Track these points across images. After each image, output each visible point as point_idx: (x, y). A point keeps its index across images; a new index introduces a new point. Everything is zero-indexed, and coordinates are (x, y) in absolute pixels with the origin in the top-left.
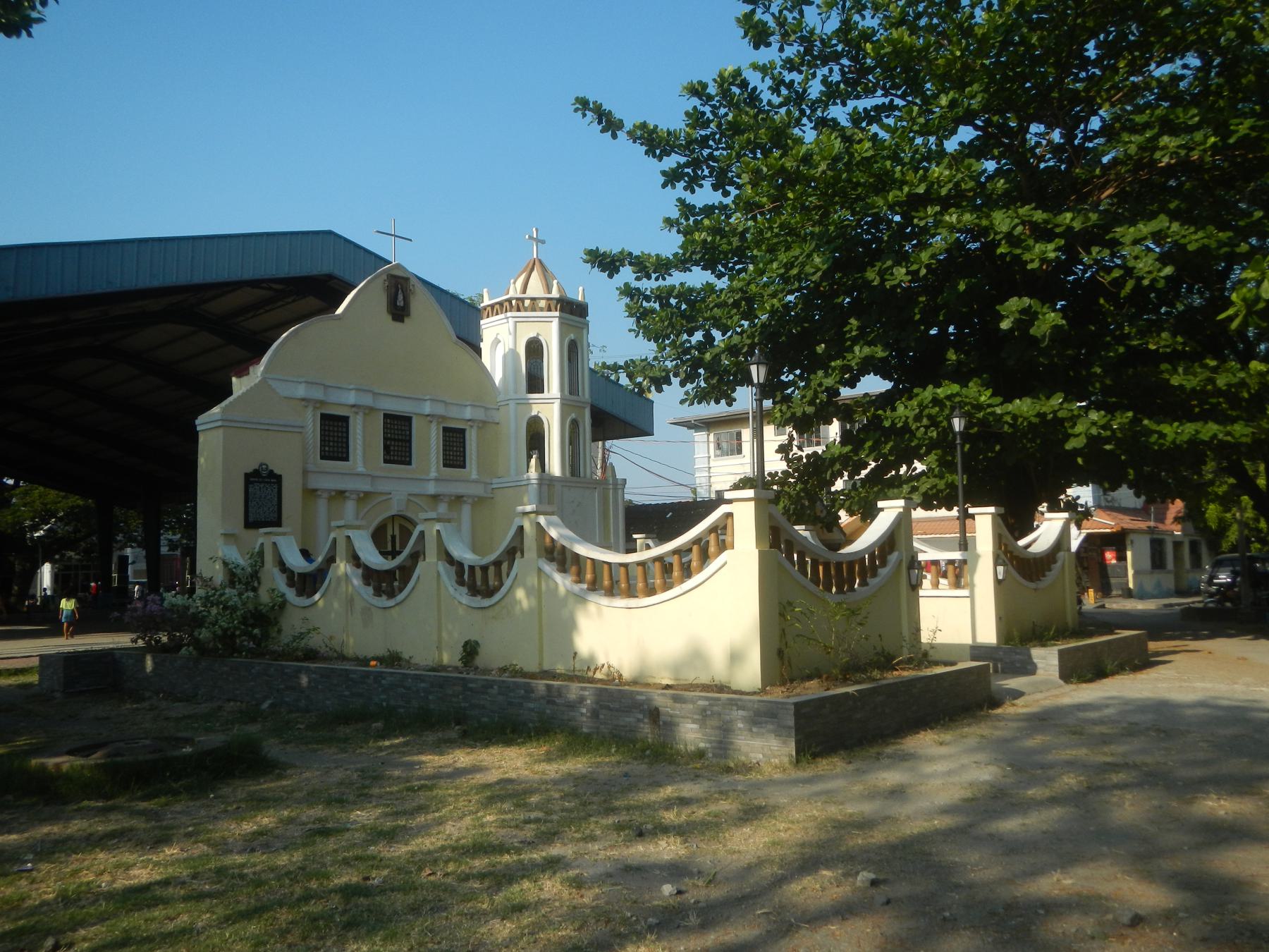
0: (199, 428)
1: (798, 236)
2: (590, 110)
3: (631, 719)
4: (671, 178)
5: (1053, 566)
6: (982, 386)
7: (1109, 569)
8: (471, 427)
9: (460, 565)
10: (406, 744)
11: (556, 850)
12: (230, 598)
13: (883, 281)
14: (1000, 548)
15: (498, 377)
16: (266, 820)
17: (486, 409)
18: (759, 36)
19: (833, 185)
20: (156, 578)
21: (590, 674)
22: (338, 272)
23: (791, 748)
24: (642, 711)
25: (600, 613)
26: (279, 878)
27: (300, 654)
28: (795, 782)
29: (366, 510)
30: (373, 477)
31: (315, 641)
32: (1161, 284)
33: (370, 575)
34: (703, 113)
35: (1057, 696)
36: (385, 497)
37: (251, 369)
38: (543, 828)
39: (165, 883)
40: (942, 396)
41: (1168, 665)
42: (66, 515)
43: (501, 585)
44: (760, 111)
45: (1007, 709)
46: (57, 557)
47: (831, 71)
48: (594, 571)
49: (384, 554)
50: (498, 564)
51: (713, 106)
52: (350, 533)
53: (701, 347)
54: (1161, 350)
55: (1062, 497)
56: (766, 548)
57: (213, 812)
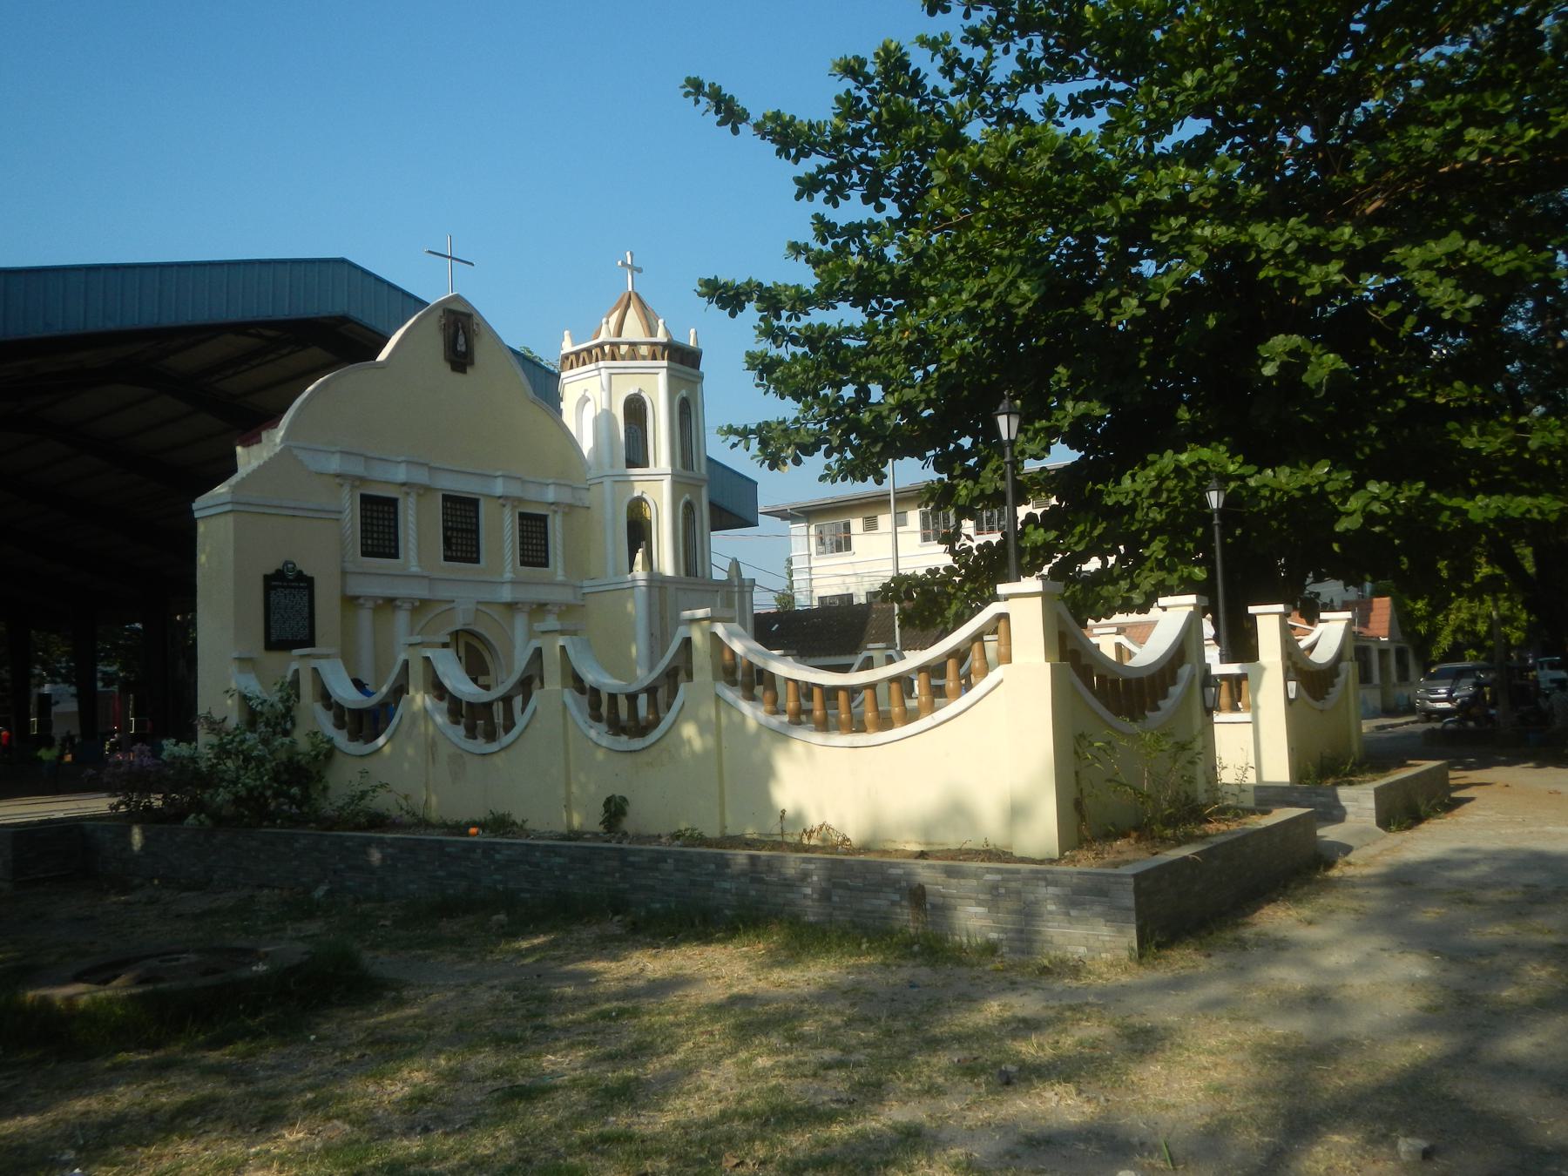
0: (197, 515)
2: (705, 95)
4: (807, 187)
5: (1336, 680)
8: (555, 512)
9: (595, 692)
10: (554, 945)
12: (254, 747)
15: (587, 445)
17: (574, 488)
23: (1131, 937)
24: (899, 890)
25: (810, 754)
27: (363, 820)
29: (423, 622)
30: (431, 579)
31: (382, 802)
32: (1467, 318)
33: (458, 709)
34: (859, 100)
36: (448, 606)
37: (264, 435)
40: (1186, 464)
41: (1472, 803)
47: (1030, 43)
50: (507, 700)
51: (872, 91)
52: (429, 653)
54: (1452, 404)
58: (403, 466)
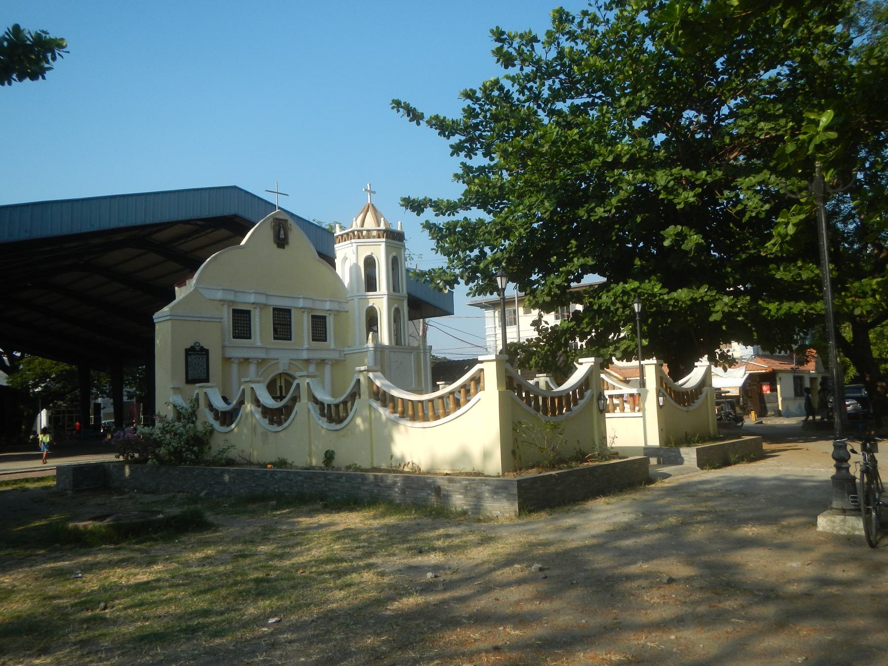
0: (155, 321)
1: (537, 186)
2: (402, 107)
3: (424, 494)
4: (457, 149)
6: (657, 281)
7: (765, 397)
10: (290, 513)
11: (373, 560)
12: (178, 428)
13: (589, 216)
14: (662, 386)
15: (346, 282)
16: (210, 552)
17: (339, 302)
18: (508, 61)
19: (556, 156)
20: (121, 416)
21: (402, 468)
22: (241, 213)
25: (407, 431)
26: (220, 576)
28: (515, 525)
30: (267, 349)
31: (233, 454)
33: (267, 412)
34: (474, 109)
35: (691, 477)
36: (276, 361)
37: (187, 282)
38: (366, 550)
39: (158, 580)
41: (775, 458)
42: (57, 376)
43: (348, 415)
44: (512, 105)
45: (659, 485)
46: (51, 405)
47: (554, 82)
48: (403, 406)
49: (275, 398)
50: (345, 403)
52: (253, 385)
53: (478, 259)
55: (717, 350)
56: (504, 389)
57: (178, 549)
58: (253, 295)
